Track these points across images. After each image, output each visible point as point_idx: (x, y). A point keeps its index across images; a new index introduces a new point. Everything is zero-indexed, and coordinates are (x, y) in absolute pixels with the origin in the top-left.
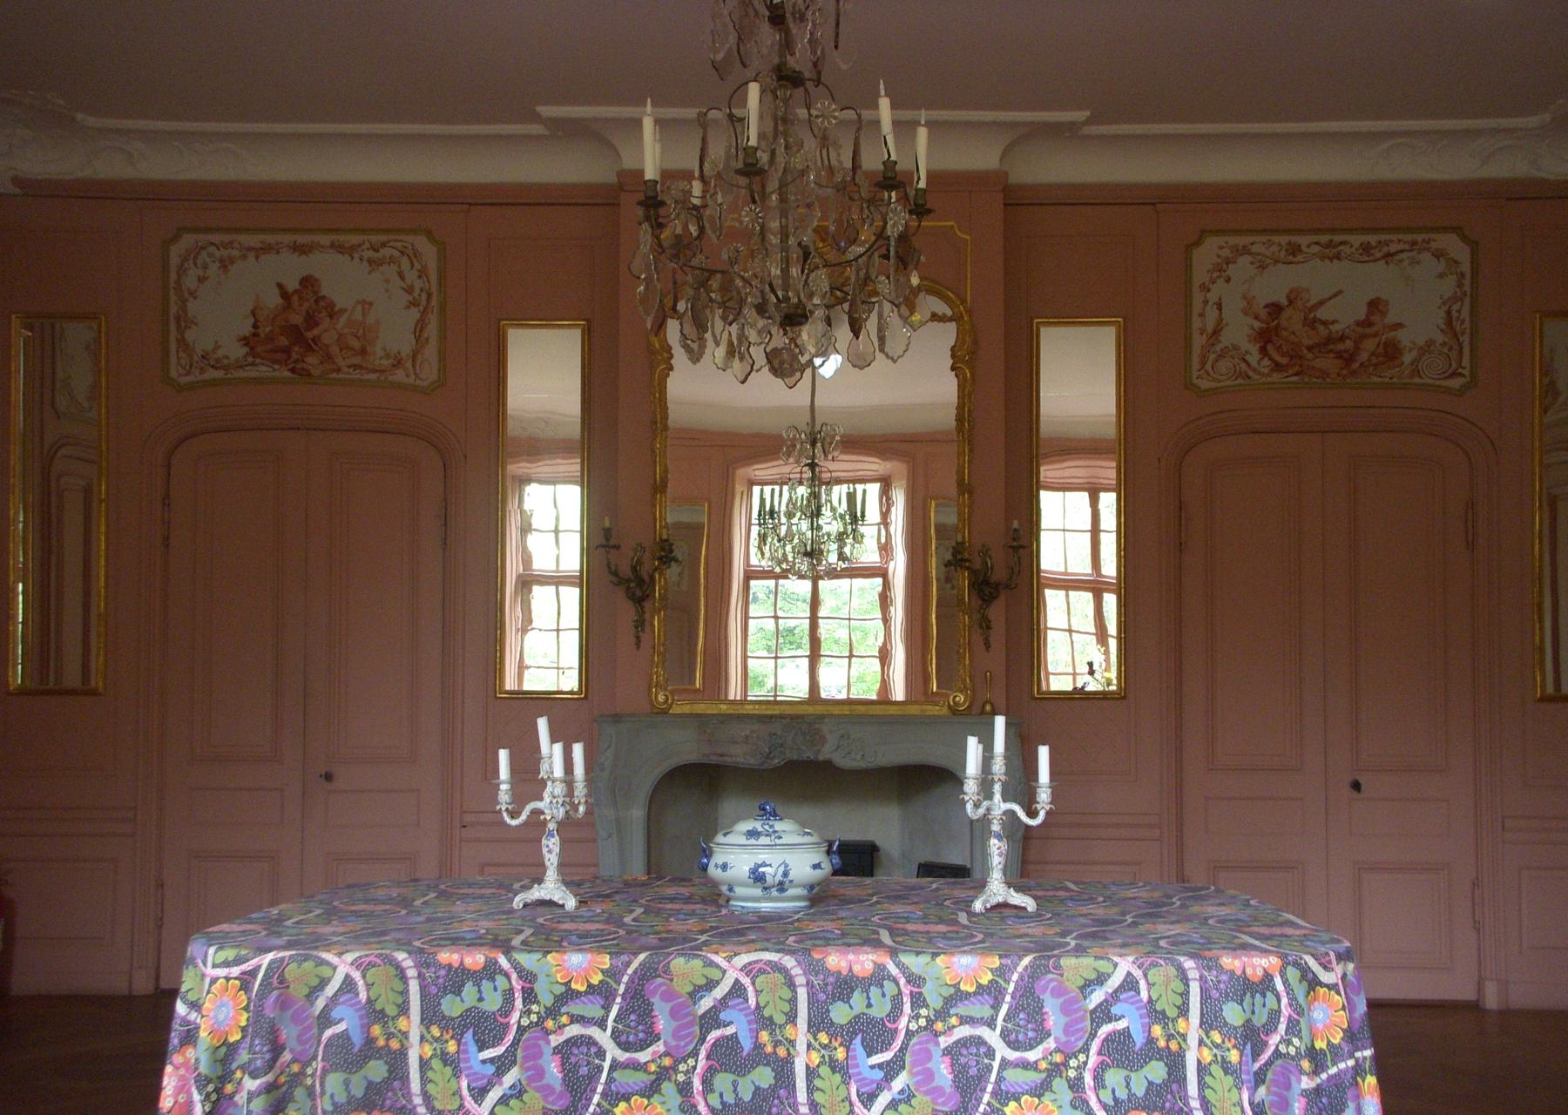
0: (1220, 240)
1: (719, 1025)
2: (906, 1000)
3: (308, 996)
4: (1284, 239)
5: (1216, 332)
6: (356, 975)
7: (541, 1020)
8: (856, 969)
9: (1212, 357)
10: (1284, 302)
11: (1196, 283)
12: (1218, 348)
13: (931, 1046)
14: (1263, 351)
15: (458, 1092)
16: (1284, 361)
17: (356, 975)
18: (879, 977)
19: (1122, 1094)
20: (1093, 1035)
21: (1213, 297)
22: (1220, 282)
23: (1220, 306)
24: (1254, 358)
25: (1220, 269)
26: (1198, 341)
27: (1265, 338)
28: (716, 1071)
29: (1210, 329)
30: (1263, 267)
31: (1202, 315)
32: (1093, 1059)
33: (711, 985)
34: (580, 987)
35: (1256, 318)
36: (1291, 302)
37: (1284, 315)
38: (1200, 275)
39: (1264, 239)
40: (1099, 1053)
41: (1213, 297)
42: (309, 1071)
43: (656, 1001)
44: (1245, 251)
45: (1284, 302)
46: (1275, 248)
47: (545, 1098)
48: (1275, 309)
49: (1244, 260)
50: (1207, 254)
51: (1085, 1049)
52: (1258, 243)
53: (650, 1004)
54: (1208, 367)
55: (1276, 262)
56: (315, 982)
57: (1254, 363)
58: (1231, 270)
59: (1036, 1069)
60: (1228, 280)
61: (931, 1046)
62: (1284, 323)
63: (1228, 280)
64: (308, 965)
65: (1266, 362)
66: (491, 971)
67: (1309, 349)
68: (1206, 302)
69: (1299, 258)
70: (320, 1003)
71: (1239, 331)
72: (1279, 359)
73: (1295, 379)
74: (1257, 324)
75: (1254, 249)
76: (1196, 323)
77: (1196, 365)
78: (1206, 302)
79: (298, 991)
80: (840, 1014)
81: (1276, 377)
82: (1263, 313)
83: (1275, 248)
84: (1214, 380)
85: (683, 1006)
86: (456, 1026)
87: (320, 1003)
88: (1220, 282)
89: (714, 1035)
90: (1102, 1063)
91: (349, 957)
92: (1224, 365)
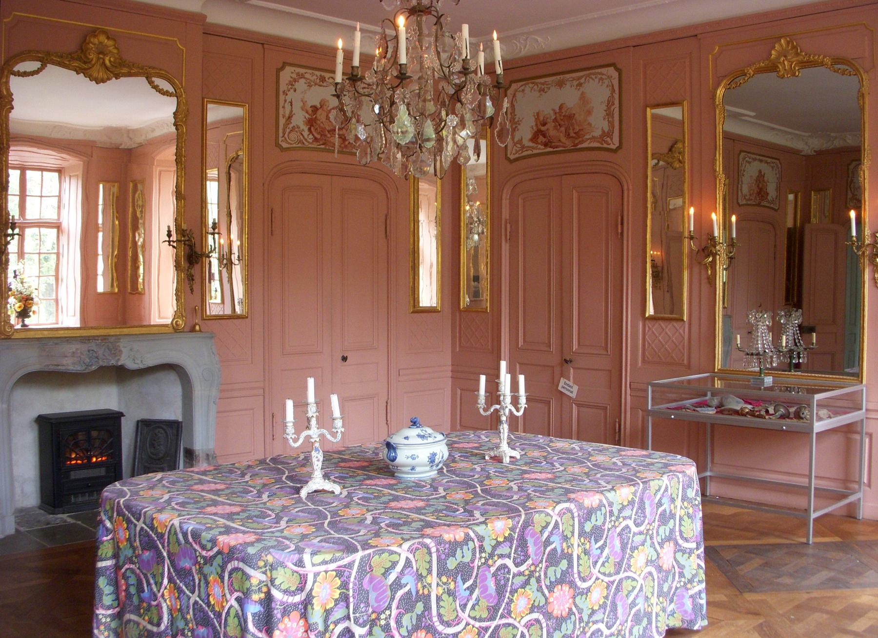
0: (292, 69)
1: (401, 587)
2: (477, 550)
3: (383, 574)
4: (318, 73)
5: (290, 117)
6: (411, 556)
7: (487, 560)
8: (457, 537)
9: (288, 131)
10: (319, 106)
11: (281, 90)
12: (291, 126)
13: (487, 573)
14: (310, 130)
15: (455, 610)
16: (318, 136)
17: (411, 556)
18: (601, 505)
19: (553, 579)
20: (393, 599)
21: (288, 98)
22: (292, 91)
23: (291, 103)
24: (306, 133)
25: (292, 83)
26: (282, 121)
27: (311, 123)
28: (403, 614)
29: (287, 115)
30: (310, 86)
31: (283, 107)
32: (394, 612)
33: (394, 564)
34: (501, 539)
35: (307, 112)
36: (321, 107)
37: (319, 112)
38: (283, 87)
39: (310, 71)
40: (397, 608)
41: (288, 98)
42: (538, 569)
43: (529, 538)
44: (302, 76)
45: (319, 106)
46: (315, 77)
47: (488, 601)
48: (315, 109)
49: (302, 81)
50: (287, 74)
51: (389, 608)
52: (308, 74)
53: (526, 541)
54: (286, 135)
55: (316, 84)
56: (389, 565)
57: (306, 137)
58: (297, 85)
59: (524, 575)
60: (295, 91)
61: (487, 573)
62: (319, 117)
63: (295, 91)
64: (385, 555)
65: (311, 136)
66: (468, 539)
67: (329, 131)
68: (285, 101)
69: (325, 84)
70: (546, 535)
71: (300, 119)
72: (316, 135)
73: (323, 146)
74: (307, 116)
75: (307, 76)
76: (281, 111)
77: (281, 134)
78: (285, 101)
79: (378, 572)
80: (452, 564)
81: (315, 145)
82: (310, 110)
83: (315, 77)
84: (289, 143)
85: (380, 582)
86: (452, 575)
87: (546, 535)
88: (292, 91)
89: (400, 593)
90: (400, 613)
91: (406, 545)
92: (293, 136)
